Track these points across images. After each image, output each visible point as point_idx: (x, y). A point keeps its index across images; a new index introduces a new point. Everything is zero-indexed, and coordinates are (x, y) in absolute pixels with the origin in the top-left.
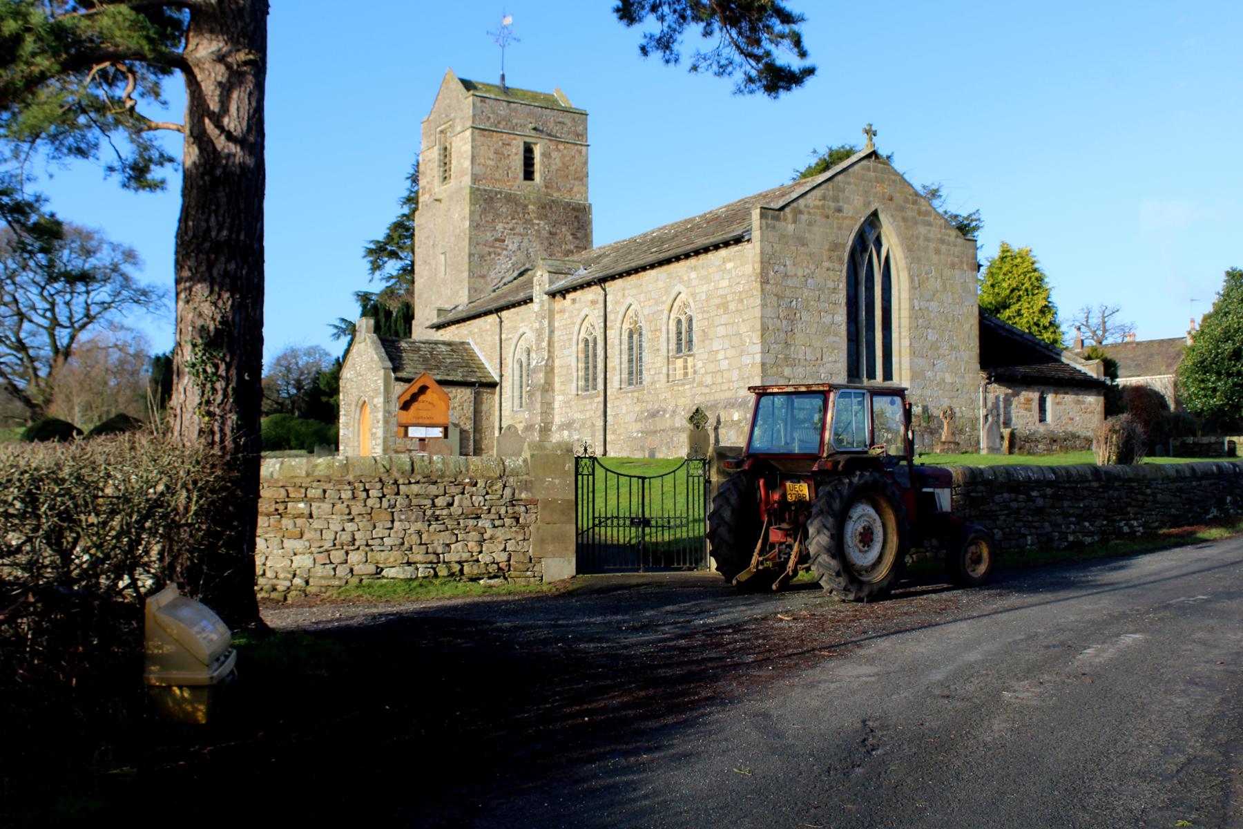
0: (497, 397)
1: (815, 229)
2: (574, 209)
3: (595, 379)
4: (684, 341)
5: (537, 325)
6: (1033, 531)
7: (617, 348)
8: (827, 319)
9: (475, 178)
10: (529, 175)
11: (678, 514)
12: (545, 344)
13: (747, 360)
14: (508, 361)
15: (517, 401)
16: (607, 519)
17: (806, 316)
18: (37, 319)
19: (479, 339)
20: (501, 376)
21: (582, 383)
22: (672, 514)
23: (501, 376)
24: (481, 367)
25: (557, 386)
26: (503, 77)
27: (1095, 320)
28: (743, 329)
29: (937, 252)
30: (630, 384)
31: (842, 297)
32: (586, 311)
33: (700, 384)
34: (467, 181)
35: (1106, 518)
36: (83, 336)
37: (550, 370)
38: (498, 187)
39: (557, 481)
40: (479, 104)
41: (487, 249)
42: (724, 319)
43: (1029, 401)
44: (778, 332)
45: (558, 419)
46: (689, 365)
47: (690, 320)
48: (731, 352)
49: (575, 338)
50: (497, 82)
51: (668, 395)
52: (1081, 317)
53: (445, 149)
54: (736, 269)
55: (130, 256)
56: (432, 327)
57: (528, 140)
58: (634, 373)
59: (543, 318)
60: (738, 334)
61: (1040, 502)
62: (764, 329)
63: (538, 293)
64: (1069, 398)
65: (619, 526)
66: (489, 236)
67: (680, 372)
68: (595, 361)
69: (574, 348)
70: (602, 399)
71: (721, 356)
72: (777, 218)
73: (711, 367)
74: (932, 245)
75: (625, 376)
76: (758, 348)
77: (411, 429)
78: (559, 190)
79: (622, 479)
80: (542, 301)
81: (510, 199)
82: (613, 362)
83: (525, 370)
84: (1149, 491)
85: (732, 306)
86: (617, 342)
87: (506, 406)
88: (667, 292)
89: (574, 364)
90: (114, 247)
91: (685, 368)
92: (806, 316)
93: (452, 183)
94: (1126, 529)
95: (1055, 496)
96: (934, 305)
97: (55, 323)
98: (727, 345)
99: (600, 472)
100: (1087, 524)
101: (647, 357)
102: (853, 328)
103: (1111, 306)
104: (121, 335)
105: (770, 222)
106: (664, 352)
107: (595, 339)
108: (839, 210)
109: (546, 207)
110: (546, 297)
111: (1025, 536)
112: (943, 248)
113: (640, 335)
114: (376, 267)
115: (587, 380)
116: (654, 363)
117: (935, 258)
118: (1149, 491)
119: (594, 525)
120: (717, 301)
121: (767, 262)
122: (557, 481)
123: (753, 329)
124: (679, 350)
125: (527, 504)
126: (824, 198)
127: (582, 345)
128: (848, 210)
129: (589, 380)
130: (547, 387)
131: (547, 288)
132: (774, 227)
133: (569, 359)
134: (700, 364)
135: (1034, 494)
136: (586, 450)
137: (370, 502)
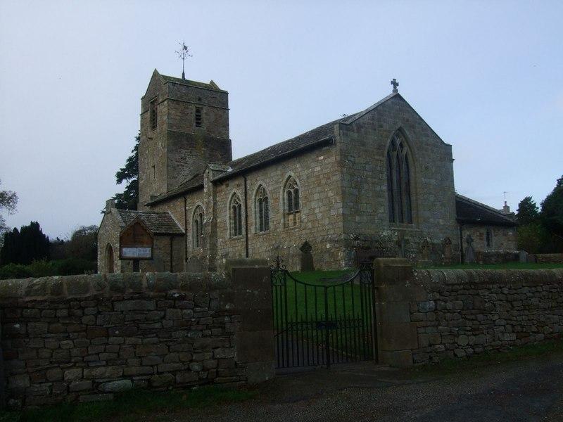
0: (185, 243)
2: (222, 142)
3: (240, 228)
4: (293, 204)
5: (206, 200)
7: (253, 210)
9: (170, 126)
10: (198, 124)
12: (211, 210)
13: (333, 213)
14: (191, 221)
15: (195, 243)
16: (297, 323)
17: (366, 187)
19: (174, 213)
20: (186, 230)
21: (233, 231)
22: (352, 317)
23: (186, 230)
24: (175, 225)
25: (219, 234)
26: (183, 74)
28: (330, 194)
30: (261, 230)
31: (385, 177)
32: (234, 190)
33: (305, 228)
34: (165, 127)
35: (175, 299)
37: (214, 225)
39: (256, 292)
40: (172, 87)
41: (176, 163)
43: (481, 234)
44: (352, 196)
46: (297, 218)
47: (297, 191)
49: (228, 205)
51: (285, 235)
53: (154, 111)
54: (323, 164)
56: (148, 205)
57: (198, 106)
58: (264, 224)
59: (210, 196)
62: (344, 193)
63: (208, 186)
64: (501, 232)
65: (298, 330)
66: (178, 157)
67: (291, 223)
68: (240, 218)
69: (228, 212)
70: (244, 239)
71: (317, 211)
73: (311, 218)
75: (258, 226)
76: (340, 205)
78: (214, 133)
79: (298, 284)
80: (208, 186)
82: (252, 219)
83: (199, 225)
85: (323, 182)
86: (253, 207)
87: (190, 246)
88: (282, 175)
89: (228, 221)
91: (295, 219)
92: (366, 187)
93: (158, 130)
96: (433, 181)
99: (290, 283)
101: (271, 215)
102: (390, 193)
105: (345, 132)
107: (240, 206)
108: (382, 126)
110: (210, 184)
113: (267, 202)
114: (119, 181)
115: (235, 230)
120: (314, 179)
121: (344, 154)
122: (256, 292)
123: (337, 194)
124: (290, 209)
125: (230, 313)
126: (373, 119)
127: (232, 210)
129: (237, 229)
130: (214, 234)
131: (212, 179)
133: (226, 217)
134: (304, 217)
136: (278, 264)
137: (85, 320)
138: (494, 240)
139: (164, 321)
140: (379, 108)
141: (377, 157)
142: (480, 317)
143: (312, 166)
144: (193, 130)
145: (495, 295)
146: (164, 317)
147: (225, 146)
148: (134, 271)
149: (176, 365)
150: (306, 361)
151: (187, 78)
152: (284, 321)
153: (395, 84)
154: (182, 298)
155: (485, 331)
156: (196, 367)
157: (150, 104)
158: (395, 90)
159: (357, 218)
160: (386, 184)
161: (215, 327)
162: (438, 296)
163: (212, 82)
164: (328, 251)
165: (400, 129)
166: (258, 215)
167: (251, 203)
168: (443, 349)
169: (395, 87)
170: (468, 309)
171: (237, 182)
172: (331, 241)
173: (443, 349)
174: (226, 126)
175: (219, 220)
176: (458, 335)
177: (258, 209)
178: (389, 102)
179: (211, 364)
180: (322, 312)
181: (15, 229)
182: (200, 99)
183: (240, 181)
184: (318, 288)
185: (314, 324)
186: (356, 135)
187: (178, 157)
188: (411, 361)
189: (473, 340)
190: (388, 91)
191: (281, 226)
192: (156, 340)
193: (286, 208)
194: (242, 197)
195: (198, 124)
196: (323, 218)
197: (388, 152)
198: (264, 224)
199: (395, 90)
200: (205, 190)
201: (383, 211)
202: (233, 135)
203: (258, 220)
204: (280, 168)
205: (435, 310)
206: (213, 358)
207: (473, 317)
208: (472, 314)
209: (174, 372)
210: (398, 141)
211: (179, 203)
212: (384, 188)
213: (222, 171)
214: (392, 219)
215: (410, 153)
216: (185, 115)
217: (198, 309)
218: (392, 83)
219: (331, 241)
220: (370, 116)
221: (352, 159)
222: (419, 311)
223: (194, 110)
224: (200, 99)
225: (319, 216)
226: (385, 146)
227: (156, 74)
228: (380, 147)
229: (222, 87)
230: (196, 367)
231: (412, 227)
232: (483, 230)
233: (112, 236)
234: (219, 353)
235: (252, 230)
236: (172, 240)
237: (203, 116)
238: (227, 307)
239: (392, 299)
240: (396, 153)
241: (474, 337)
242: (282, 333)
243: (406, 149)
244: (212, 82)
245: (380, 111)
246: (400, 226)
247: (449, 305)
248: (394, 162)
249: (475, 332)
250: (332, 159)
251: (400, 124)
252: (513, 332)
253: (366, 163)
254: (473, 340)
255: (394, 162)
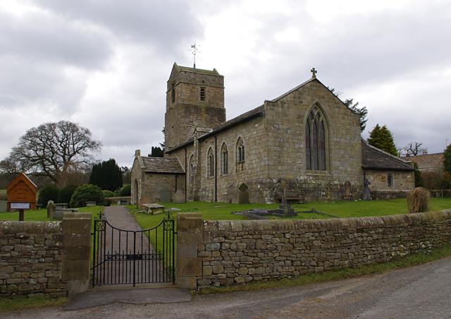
1: (291, 110)
6: (372, 252)
8: (297, 146)
11: (151, 252)
16: (112, 256)
17: (287, 145)
18: (59, 153)
21: (210, 173)
22: (147, 253)
25: (202, 174)
27: (414, 148)
29: (343, 119)
31: (303, 137)
32: (210, 146)
35: (21, 238)
36: (72, 158)
38: (191, 103)
39: (79, 235)
42: (255, 147)
43: (383, 178)
45: (202, 187)
47: (243, 148)
48: (257, 160)
50: (193, 67)
52: (409, 147)
55: (87, 132)
58: (226, 171)
60: (260, 153)
61: (375, 237)
64: (401, 176)
71: (254, 162)
72: (274, 106)
74: (341, 116)
75: (223, 170)
77: (12, 204)
81: (196, 107)
82: (219, 166)
84: (435, 225)
88: (236, 137)
90: (82, 129)
92: (287, 145)
94: (423, 246)
95: (384, 233)
96: (343, 140)
97: (65, 154)
98: (256, 157)
99: (109, 229)
100: (402, 246)
103: (419, 142)
104: (87, 158)
106: (235, 161)
108: (301, 102)
109: (208, 110)
111: (367, 256)
112: (346, 117)
116: (232, 165)
117: (342, 121)
118: (435, 225)
119: (105, 260)
120: (252, 140)
122: (79, 235)
125: (59, 248)
126: (294, 98)
128: (305, 102)
132: (273, 109)
133: (205, 163)
135: (373, 232)
138: (394, 181)
139: (12, 252)
140: (299, 90)
141: (297, 124)
142: (261, 255)
143: (252, 130)
144: (198, 102)
145: (278, 239)
146: (13, 250)
147: (221, 112)
148: (20, 220)
149: (19, 280)
150: (154, 279)
151: (197, 67)
152: (103, 253)
153: (314, 71)
154: (25, 238)
155: (265, 265)
156: (32, 281)
157: (172, 84)
158: (314, 76)
159: (280, 168)
160: (304, 143)
161: (47, 257)
162: (223, 239)
163: (214, 69)
164: (259, 190)
165: (317, 104)
166: (223, 163)
167: (219, 154)
168: (225, 277)
169: (314, 74)
170: (251, 249)
171: (211, 140)
172: (261, 183)
173: (225, 277)
174: (222, 99)
175: (202, 165)
176: (239, 267)
177: (223, 159)
178: (308, 85)
179: (43, 280)
180: (131, 246)
181: (362, 113)
182: (203, 82)
183: (213, 140)
184: (137, 233)
185: (125, 257)
186: (280, 109)
187: (187, 120)
188: (195, 285)
189: (252, 271)
190: (309, 77)
191: (235, 171)
192: (6, 263)
193: (238, 159)
194: (214, 150)
195: (202, 99)
196: (257, 168)
197: (308, 120)
198: (226, 171)
199: (314, 76)
200: (195, 145)
201: (302, 162)
202: (226, 106)
203: (223, 166)
204: (234, 131)
205: (220, 250)
206: (45, 276)
207: (255, 255)
208: (254, 252)
209: (17, 284)
210: (316, 113)
211: (183, 152)
212: (303, 145)
213: (205, 132)
214: (309, 168)
215: (324, 119)
216: (194, 93)
217: (36, 245)
218: (312, 71)
219: (261, 183)
220: (292, 95)
221: (277, 126)
222: (205, 250)
223: (200, 89)
224: (203, 82)
225: (255, 165)
226: (303, 116)
227: (175, 65)
228: (300, 117)
229: (220, 73)
230: (32, 281)
231: (325, 173)
232: (385, 175)
233: (137, 175)
234: (49, 274)
235: (219, 173)
236: (176, 177)
237: (206, 93)
238: (57, 244)
239: (184, 241)
240: (313, 121)
241: (253, 269)
242: (101, 264)
243: (322, 117)
244: (214, 69)
245: (299, 92)
246: (315, 172)
247: (233, 246)
248: (312, 127)
249: (255, 265)
250: (263, 126)
251: (317, 100)
252: (292, 265)
253: (288, 129)
254: (252, 271)
255: (312, 127)
